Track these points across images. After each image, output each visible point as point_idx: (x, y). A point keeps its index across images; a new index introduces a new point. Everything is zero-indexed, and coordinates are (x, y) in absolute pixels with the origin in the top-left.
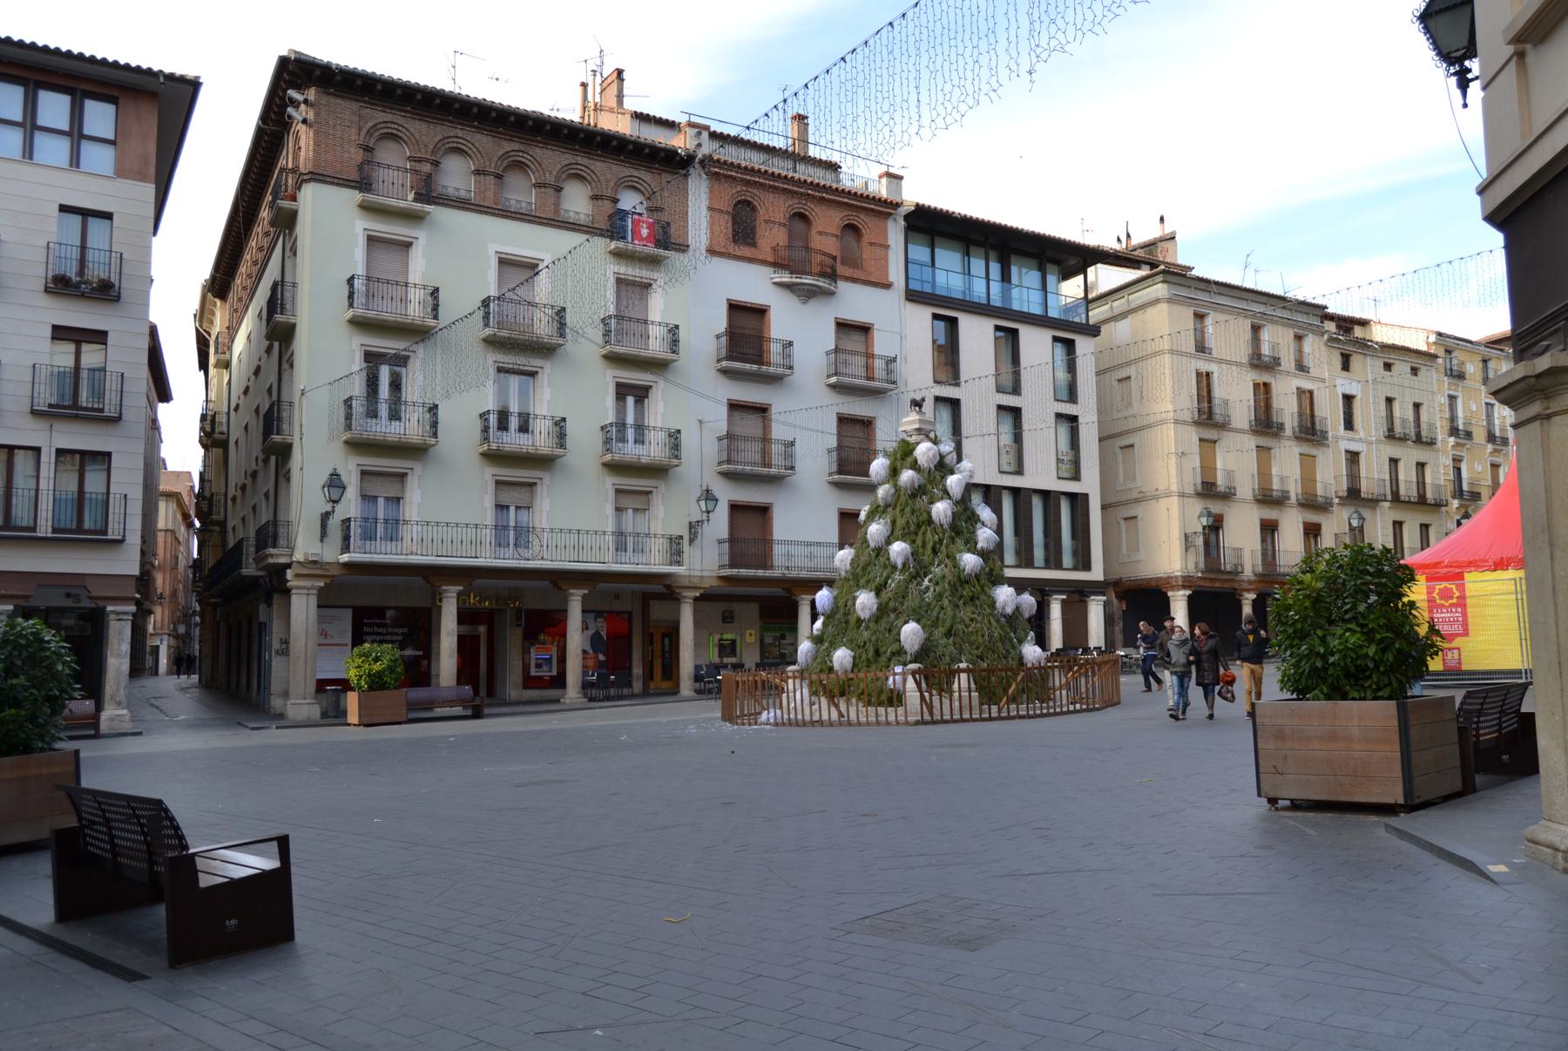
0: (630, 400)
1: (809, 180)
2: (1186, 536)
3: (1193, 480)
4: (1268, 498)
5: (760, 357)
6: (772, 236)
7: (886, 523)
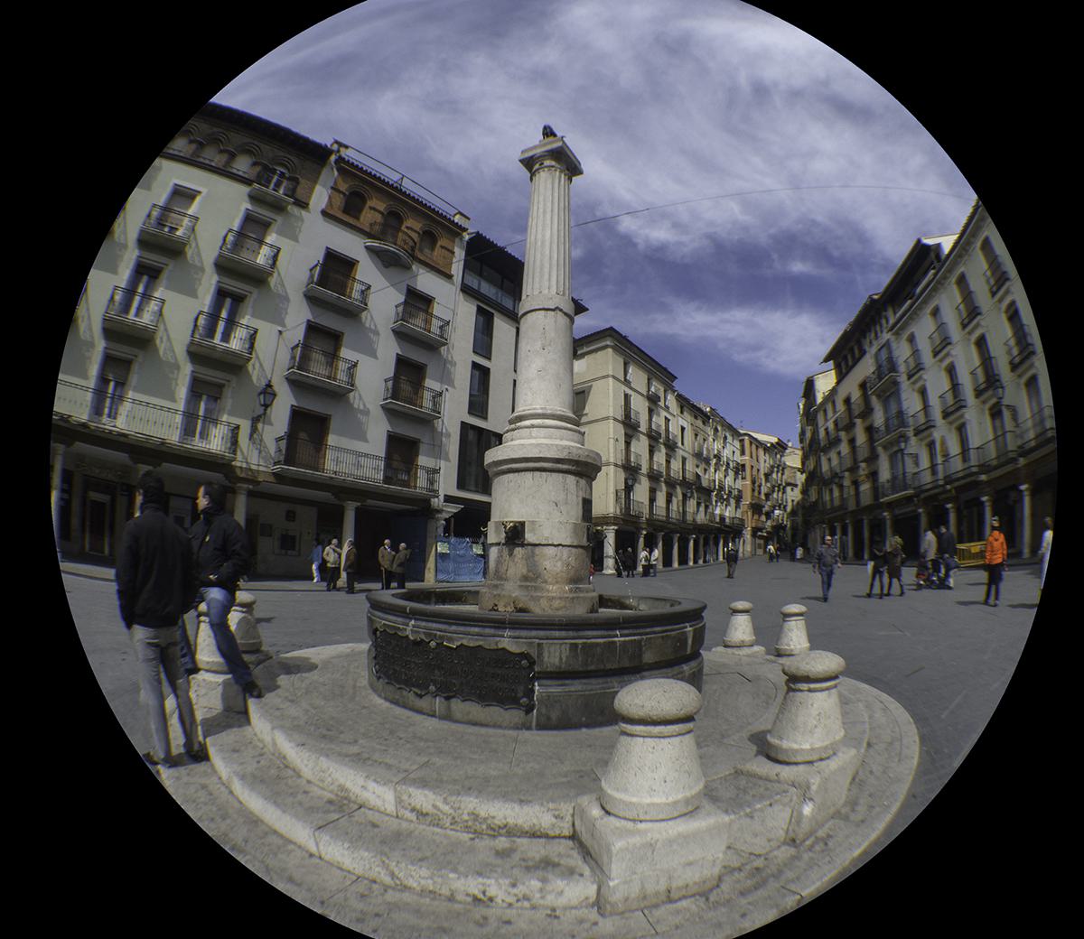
0: (228, 301)
1: (395, 185)
2: (617, 491)
3: (620, 459)
4: (631, 470)
5: (342, 289)
6: (368, 217)
7: (376, 198)
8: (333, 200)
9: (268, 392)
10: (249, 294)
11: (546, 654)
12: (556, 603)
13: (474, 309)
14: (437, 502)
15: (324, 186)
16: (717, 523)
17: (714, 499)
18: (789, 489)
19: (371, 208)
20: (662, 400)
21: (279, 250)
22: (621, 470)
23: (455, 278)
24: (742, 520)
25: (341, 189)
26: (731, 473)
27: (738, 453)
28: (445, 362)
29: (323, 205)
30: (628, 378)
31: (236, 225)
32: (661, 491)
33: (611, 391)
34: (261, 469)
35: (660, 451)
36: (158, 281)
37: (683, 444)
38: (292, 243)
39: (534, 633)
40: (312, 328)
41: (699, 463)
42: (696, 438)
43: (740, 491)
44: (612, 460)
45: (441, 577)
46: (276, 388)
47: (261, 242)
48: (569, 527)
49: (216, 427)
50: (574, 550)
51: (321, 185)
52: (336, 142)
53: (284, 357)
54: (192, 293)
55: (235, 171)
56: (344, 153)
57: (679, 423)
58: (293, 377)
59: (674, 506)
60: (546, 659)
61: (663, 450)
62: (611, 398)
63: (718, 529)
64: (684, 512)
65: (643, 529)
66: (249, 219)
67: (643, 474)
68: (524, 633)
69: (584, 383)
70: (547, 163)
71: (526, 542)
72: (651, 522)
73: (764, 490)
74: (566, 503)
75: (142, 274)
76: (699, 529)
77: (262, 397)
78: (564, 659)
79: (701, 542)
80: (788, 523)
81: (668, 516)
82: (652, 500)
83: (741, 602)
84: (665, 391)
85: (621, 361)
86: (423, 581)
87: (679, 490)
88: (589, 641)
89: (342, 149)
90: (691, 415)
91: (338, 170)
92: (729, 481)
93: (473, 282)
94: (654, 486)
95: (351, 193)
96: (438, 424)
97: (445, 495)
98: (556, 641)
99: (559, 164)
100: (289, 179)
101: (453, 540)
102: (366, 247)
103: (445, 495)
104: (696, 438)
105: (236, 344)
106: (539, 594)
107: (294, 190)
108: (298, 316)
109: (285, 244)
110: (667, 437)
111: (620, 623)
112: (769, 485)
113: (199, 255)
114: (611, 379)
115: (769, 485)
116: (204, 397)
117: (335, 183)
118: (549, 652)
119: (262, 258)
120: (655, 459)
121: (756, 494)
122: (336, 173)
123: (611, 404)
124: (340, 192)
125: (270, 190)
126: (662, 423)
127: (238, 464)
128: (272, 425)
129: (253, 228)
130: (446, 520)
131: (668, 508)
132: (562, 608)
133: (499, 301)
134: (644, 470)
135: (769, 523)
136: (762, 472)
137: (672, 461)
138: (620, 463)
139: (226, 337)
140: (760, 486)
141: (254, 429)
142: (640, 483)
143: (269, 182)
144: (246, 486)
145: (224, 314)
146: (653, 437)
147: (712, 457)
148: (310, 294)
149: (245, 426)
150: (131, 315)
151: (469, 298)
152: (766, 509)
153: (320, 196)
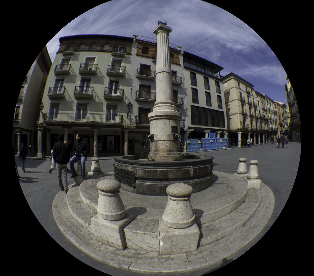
0: (114, 83)
4: (244, 115)
5: (148, 74)
8: (138, 51)
9: (130, 105)
10: (120, 80)
11: (138, 172)
12: (162, 158)
13: (189, 73)
14: (186, 129)
15: (134, 48)
16: (270, 130)
17: (269, 122)
18: (288, 118)
19: (151, 51)
20: (251, 93)
21: (125, 67)
22: (241, 115)
23: (181, 65)
24: (277, 129)
25: (140, 47)
26: (273, 114)
27: (274, 108)
28: (183, 89)
29: (136, 52)
30: (240, 87)
31: (110, 63)
32: (254, 121)
33: (235, 91)
34: (131, 125)
35: (252, 108)
36: (90, 82)
37: (259, 106)
38: (130, 64)
39: (136, 166)
40: (141, 86)
41: (264, 111)
42: (262, 104)
43: (276, 120)
44: (238, 112)
45: (188, 150)
46: (132, 103)
47: (120, 66)
48: (166, 135)
49: (117, 116)
50: (168, 142)
51: (133, 48)
52: (134, 35)
53: (134, 95)
54: (103, 83)
55: (105, 50)
56: (137, 38)
57: (257, 99)
58: (138, 100)
59: (258, 125)
60: (138, 174)
61: (253, 108)
62: (236, 94)
63: (271, 132)
64: (261, 127)
65: (250, 133)
66: (114, 61)
67: (248, 116)
68: (133, 166)
69: (227, 90)
70: (159, 31)
71: (154, 140)
72: (252, 130)
73: (282, 119)
74: (165, 128)
75: (85, 81)
76: (266, 132)
77: (128, 106)
78: (142, 174)
79: (267, 136)
80: (289, 129)
81: (256, 128)
82: (252, 123)
83: (242, 158)
84: (252, 90)
85: (237, 82)
86: (183, 152)
87: (259, 120)
88: (149, 169)
89: (136, 37)
90: (260, 97)
91: (137, 42)
92: (273, 117)
93: (188, 65)
94: (252, 119)
95: (143, 48)
96: (184, 107)
97: (188, 127)
98: (140, 169)
99: (162, 30)
100: (123, 48)
101: (191, 139)
102: (152, 61)
103: (188, 127)
104: (262, 104)
105: (119, 94)
106: (157, 155)
107: (125, 51)
108: (136, 84)
109: (127, 66)
110: (254, 104)
111: (158, 165)
112: (283, 117)
113: (101, 73)
114: (235, 88)
115: (283, 117)
116: (112, 109)
117: (138, 46)
118: (138, 172)
119: (121, 70)
120: (251, 111)
121: (280, 121)
122: (137, 44)
123: (236, 95)
124: (140, 48)
125: (118, 52)
126: (252, 100)
127: (124, 125)
128: (133, 113)
129: (116, 63)
130: (189, 134)
131: (256, 126)
132: (164, 159)
133: (197, 70)
134: (248, 114)
135: (284, 129)
136: (281, 114)
137: (256, 111)
138: (241, 113)
139: (116, 92)
140: (281, 118)
141: (128, 115)
142: (247, 119)
143: (117, 50)
144: (127, 130)
145: (114, 87)
146: (250, 104)
147: (267, 109)
148: (138, 77)
149: (125, 115)
150: (84, 92)
151: (187, 70)
152: (283, 125)
153: (134, 51)
